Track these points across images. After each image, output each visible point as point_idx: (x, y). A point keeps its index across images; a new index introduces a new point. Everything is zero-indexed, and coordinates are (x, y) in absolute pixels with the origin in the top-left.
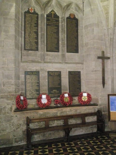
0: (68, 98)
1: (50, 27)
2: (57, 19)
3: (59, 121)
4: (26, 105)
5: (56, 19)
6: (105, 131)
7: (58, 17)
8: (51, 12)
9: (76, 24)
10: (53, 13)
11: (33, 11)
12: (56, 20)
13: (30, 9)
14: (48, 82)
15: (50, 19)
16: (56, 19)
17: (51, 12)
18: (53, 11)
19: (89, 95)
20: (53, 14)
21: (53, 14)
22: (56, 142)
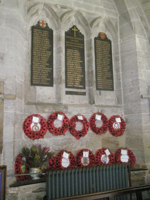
0: (119, 124)
1: (70, 50)
2: (82, 39)
3: (16, 187)
4: (25, 125)
5: (79, 39)
6: (142, 192)
7: (83, 37)
8: (73, 29)
9: (109, 59)
10: (75, 30)
11: (45, 26)
12: (79, 40)
13: (41, 23)
14: (66, 82)
15: (71, 39)
16: (79, 39)
17: (73, 29)
18: (75, 27)
19: (130, 154)
20: (75, 32)
21: (75, 32)
22: (74, 49)
